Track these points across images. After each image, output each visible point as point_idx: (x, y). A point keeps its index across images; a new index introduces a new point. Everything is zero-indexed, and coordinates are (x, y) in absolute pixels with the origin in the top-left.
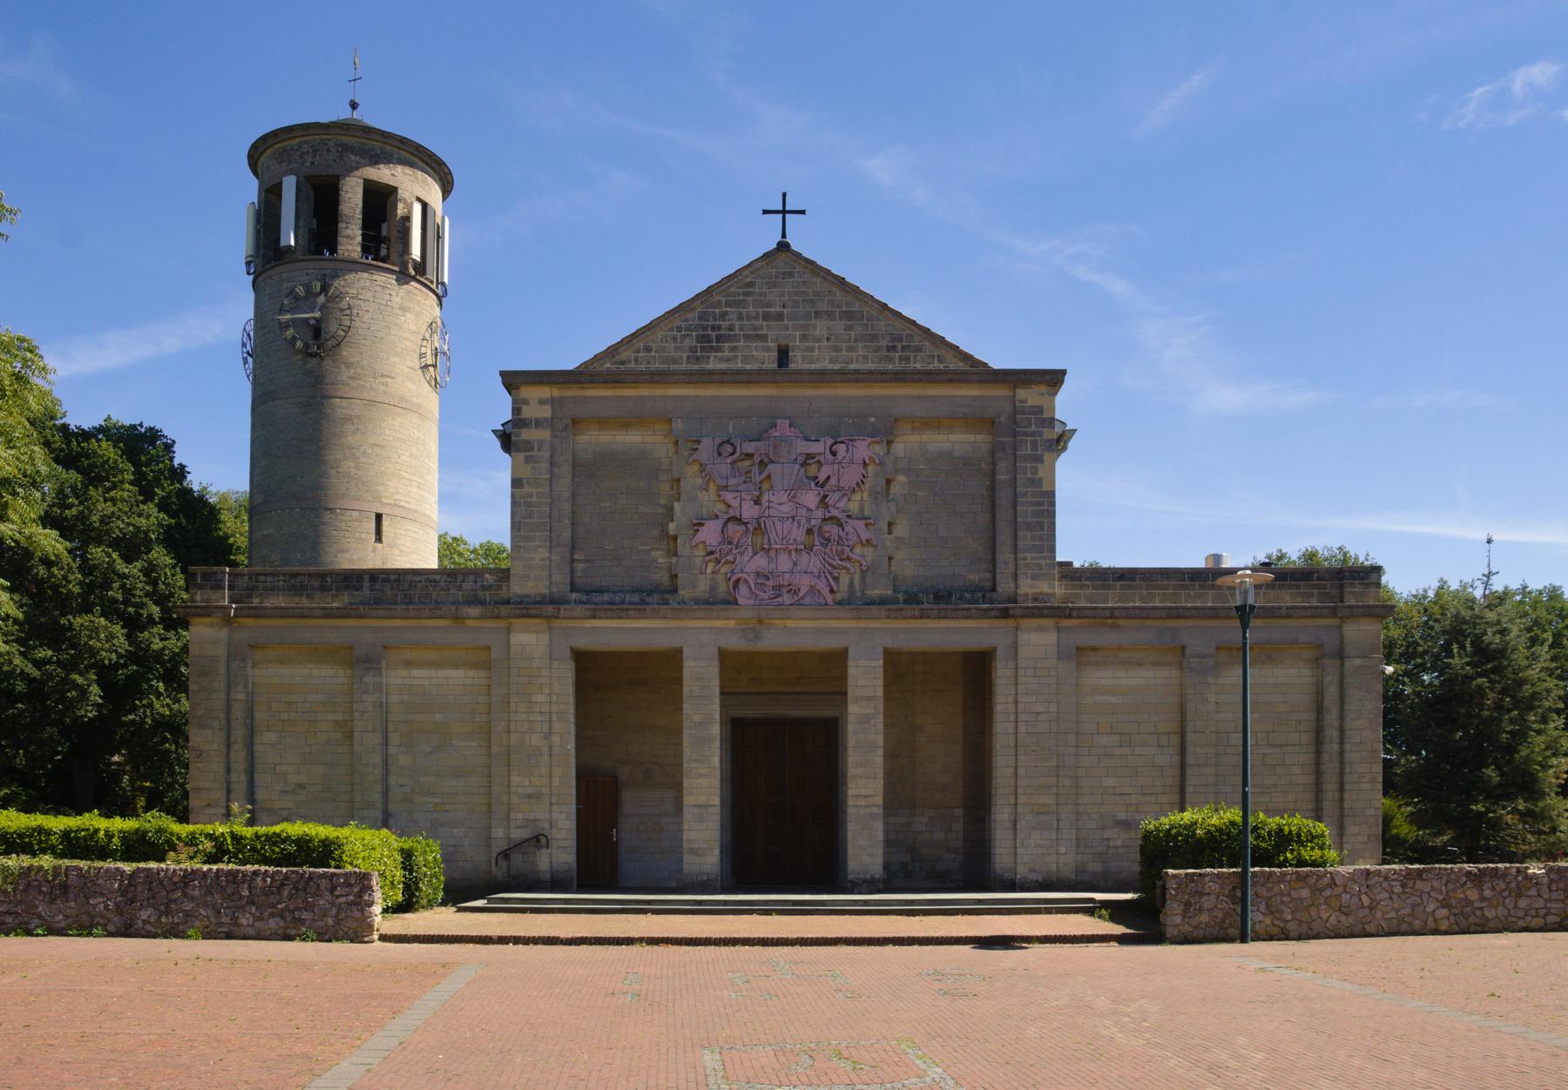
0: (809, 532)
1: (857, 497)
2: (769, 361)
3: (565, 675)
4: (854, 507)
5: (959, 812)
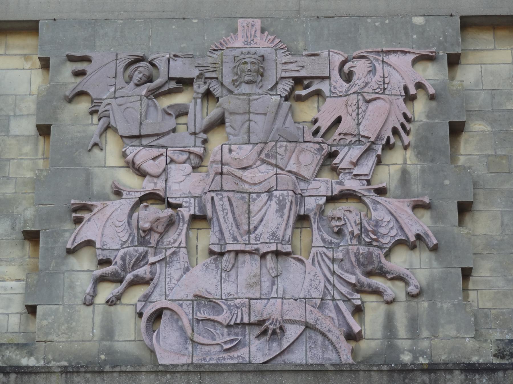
0: (302, 219)
1: (397, 157)
4: (388, 176)
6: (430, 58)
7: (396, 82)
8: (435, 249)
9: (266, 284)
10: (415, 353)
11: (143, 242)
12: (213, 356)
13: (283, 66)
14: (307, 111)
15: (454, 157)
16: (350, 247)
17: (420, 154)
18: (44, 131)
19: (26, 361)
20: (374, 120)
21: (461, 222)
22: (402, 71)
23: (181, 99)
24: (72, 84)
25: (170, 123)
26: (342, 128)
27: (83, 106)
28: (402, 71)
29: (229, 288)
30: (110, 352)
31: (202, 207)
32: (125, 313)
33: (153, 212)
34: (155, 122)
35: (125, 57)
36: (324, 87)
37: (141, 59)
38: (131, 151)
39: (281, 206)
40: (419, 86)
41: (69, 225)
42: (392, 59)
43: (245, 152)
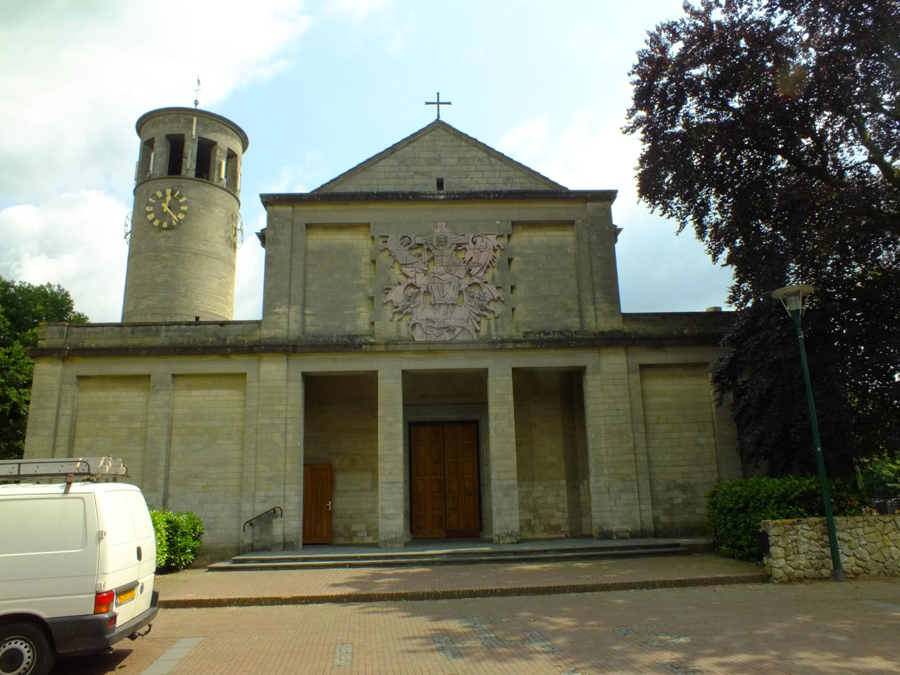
0: (460, 292)
1: (491, 271)
2: (433, 188)
3: (296, 391)
4: (488, 277)
5: (563, 482)
6: (502, 236)
7: (490, 245)
8: (503, 302)
9: (449, 314)
10: (497, 336)
11: (409, 300)
12: (432, 338)
13: (453, 239)
14: (461, 255)
15: (509, 270)
16: (475, 302)
17: (498, 269)
18: (374, 262)
19: (371, 340)
20: (484, 258)
21: (512, 292)
22: (492, 241)
23: (419, 251)
24: (383, 246)
25: (416, 259)
26: (473, 261)
27: (386, 253)
28: (492, 241)
29: (437, 315)
30: (399, 337)
31: (428, 288)
32: (403, 324)
33: (412, 290)
34: (411, 259)
35: (400, 236)
36: (467, 246)
37: (404, 237)
38: (405, 269)
39: (454, 287)
40: (498, 246)
41: (383, 295)
42: (489, 236)
43: (441, 269)
